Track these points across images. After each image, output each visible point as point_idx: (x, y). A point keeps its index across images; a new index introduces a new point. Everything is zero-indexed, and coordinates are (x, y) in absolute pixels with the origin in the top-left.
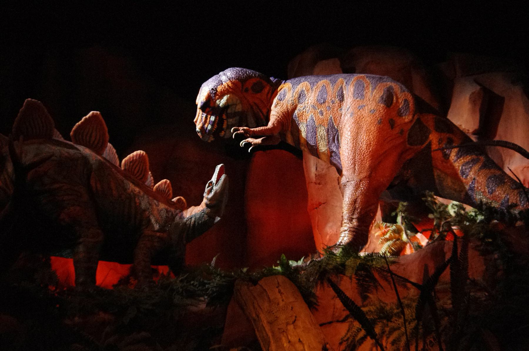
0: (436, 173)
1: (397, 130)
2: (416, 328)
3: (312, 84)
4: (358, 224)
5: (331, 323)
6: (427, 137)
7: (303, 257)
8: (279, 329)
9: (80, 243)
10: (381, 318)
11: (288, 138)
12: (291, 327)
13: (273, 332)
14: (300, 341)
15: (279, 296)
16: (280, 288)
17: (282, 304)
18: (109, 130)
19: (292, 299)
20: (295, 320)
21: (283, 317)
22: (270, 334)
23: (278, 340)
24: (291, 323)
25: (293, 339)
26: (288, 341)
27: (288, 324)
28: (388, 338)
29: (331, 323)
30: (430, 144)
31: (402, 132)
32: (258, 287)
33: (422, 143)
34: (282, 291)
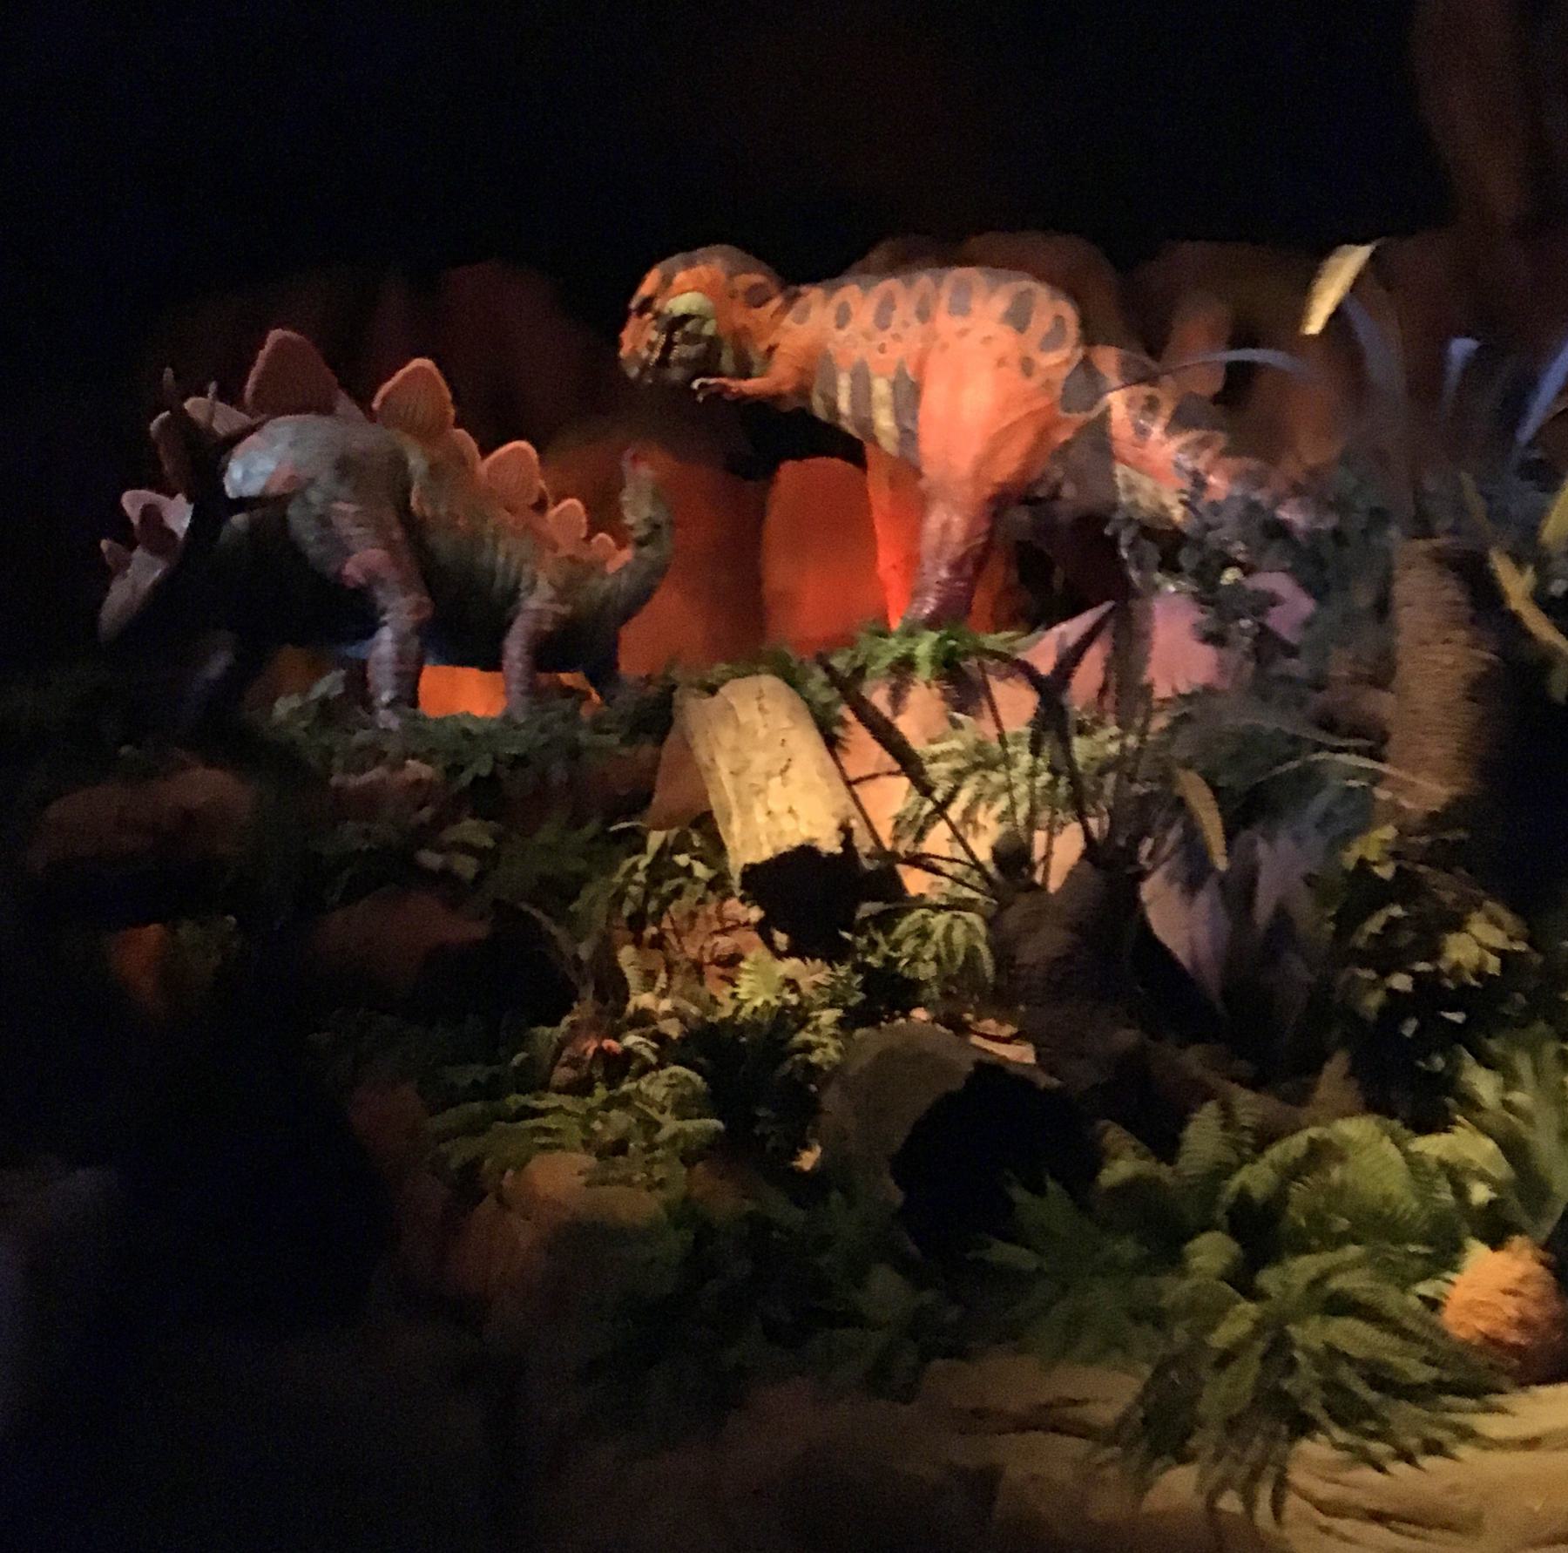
0: (1120, 470)
1: (1035, 382)
2: (1052, 785)
3: (866, 288)
4: (1118, 754)
5: (874, 776)
6: (1100, 395)
7: (1443, 1018)
8: (752, 785)
9: (385, 624)
10: (976, 766)
11: (1215, 858)
12: (776, 782)
13: (737, 792)
14: (791, 811)
15: (758, 716)
16: (764, 701)
17: (762, 733)
18: (400, 368)
19: (786, 724)
20: (787, 767)
21: (760, 760)
22: (732, 797)
23: (747, 810)
24: (778, 771)
25: (774, 806)
26: (765, 812)
27: (769, 776)
28: (989, 807)
29: (874, 776)
30: (1108, 409)
31: (1048, 384)
32: (717, 699)
33: (1089, 408)
34: (767, 706)
